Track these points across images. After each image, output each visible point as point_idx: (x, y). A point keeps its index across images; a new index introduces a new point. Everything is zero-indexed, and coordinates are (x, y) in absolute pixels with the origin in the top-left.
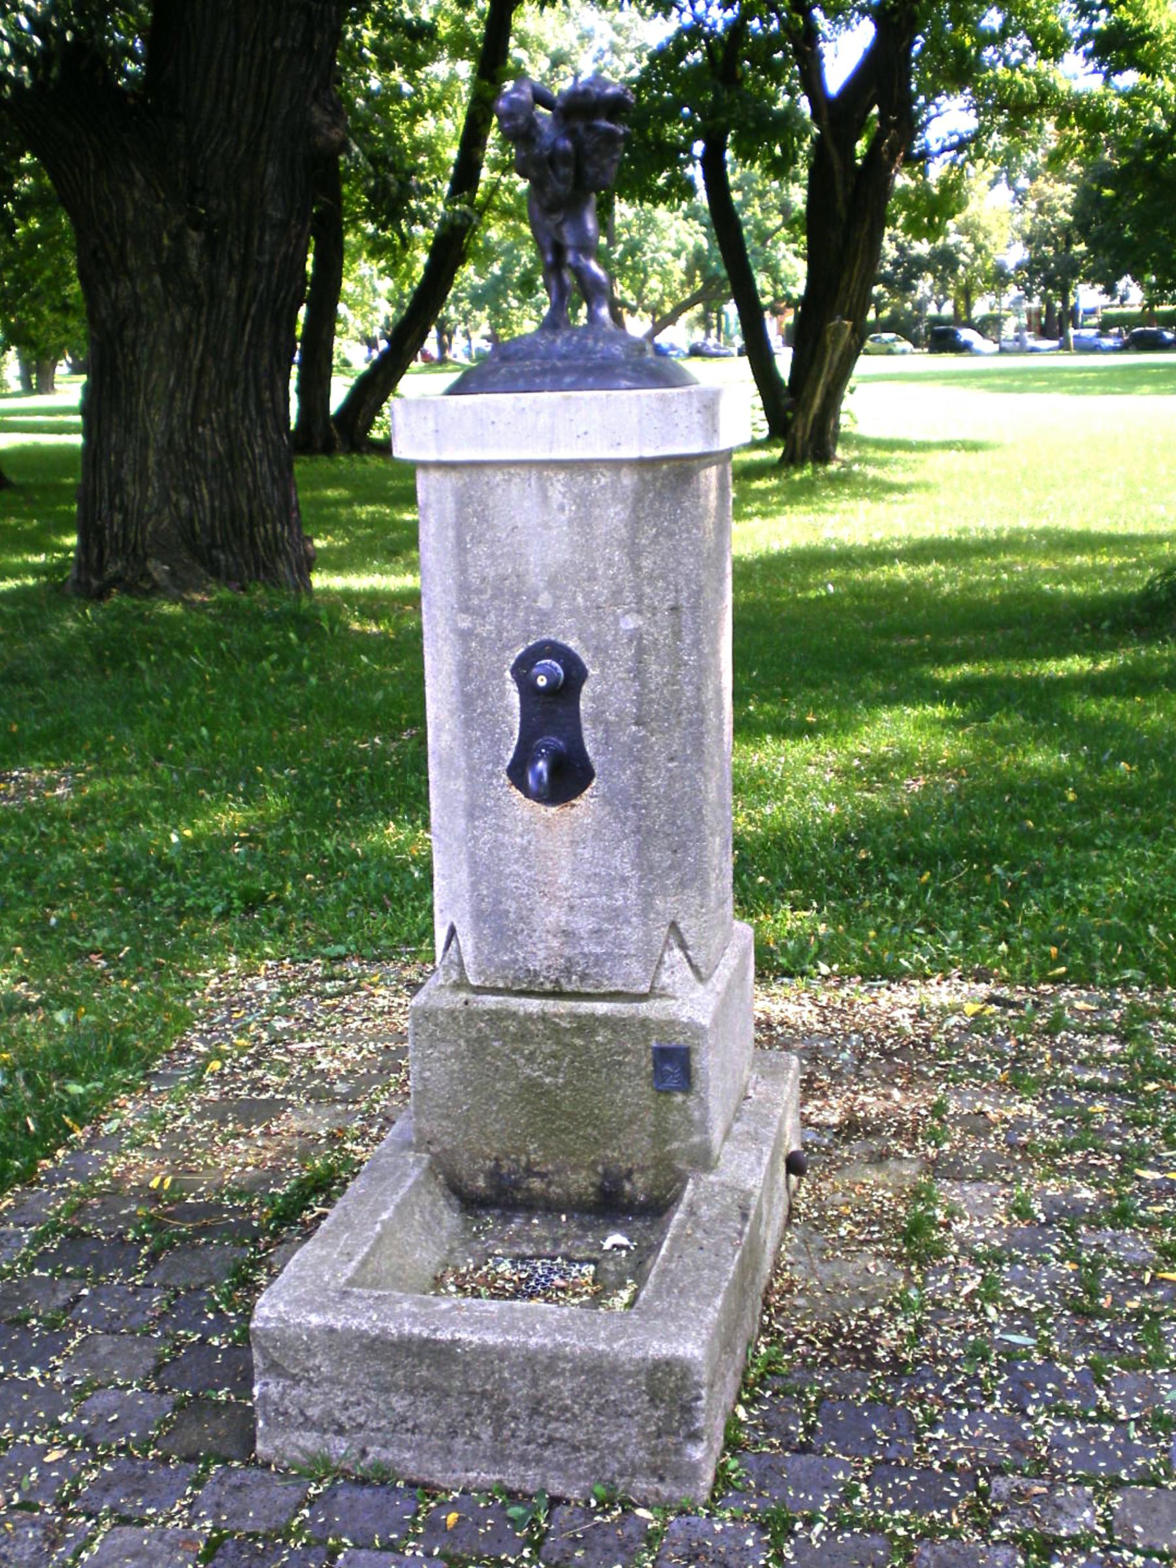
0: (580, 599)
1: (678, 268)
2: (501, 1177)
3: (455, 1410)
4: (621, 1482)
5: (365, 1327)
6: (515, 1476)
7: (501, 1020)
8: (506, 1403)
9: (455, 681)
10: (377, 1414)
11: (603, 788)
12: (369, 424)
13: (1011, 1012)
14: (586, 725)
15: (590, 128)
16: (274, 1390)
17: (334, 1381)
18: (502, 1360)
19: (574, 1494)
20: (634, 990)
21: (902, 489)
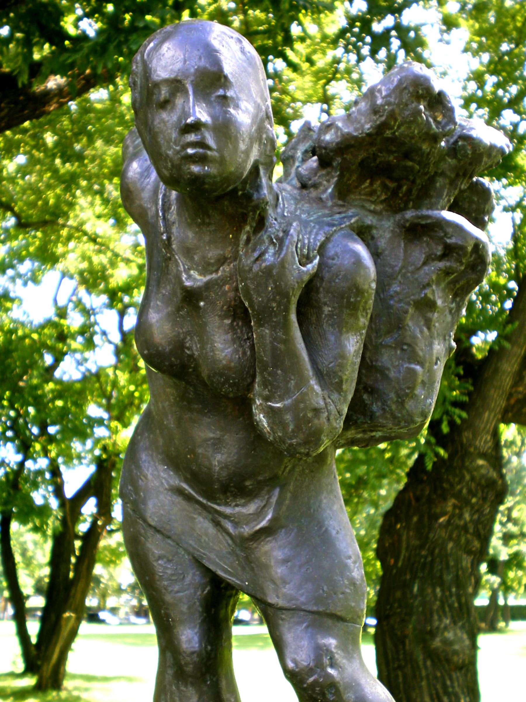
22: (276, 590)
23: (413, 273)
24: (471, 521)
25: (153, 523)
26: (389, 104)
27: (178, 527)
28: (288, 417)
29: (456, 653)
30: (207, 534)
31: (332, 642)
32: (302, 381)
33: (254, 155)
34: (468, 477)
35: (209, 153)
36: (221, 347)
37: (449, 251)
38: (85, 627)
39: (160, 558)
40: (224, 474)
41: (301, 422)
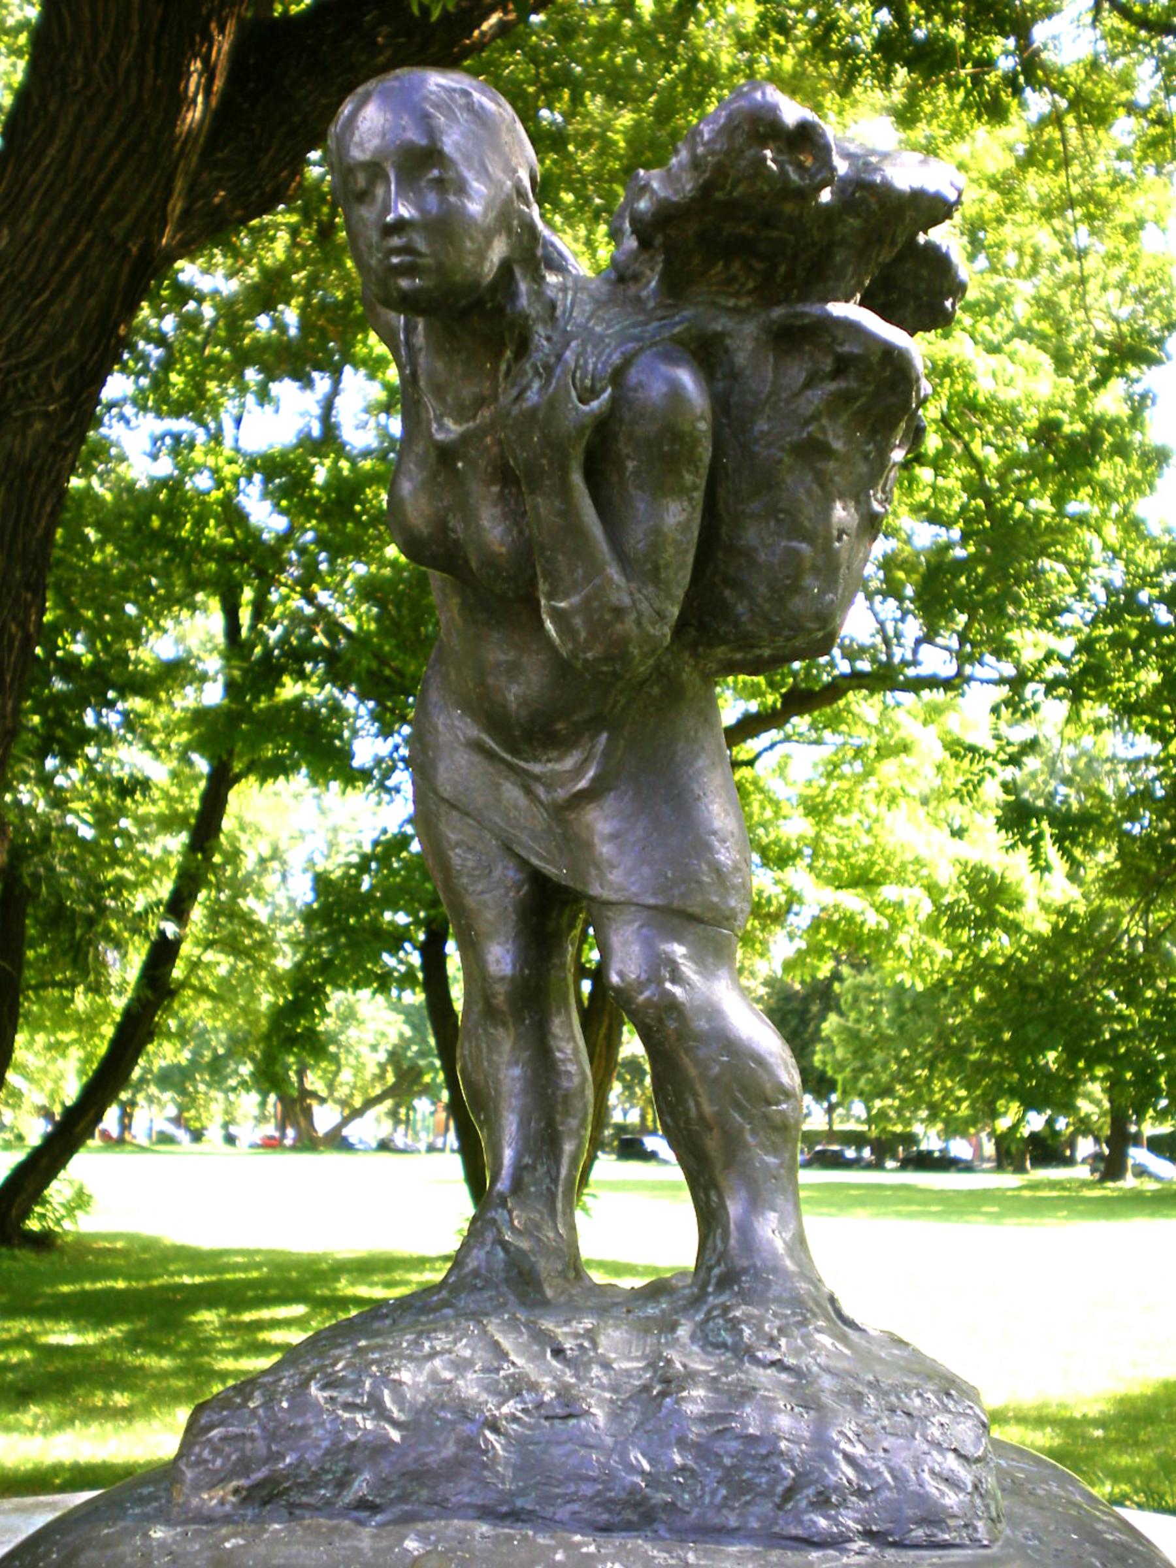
1: (372, 1061)
12: (26, 1213)
15: (793, 338)
22: (601, 878)
23: (788, 401)
25: (446, 795)
26: (713, 153)
27: (480, 800)
28: (578, 621)
30: (516, 807)
31: (679, 950)
32: (595, 569)
33: (499, 250)
35: (420, 261)
37: (843, 365)
38: (606, 1166)
39: (458, 844)
40: (524, 712)
41: (597, 628)
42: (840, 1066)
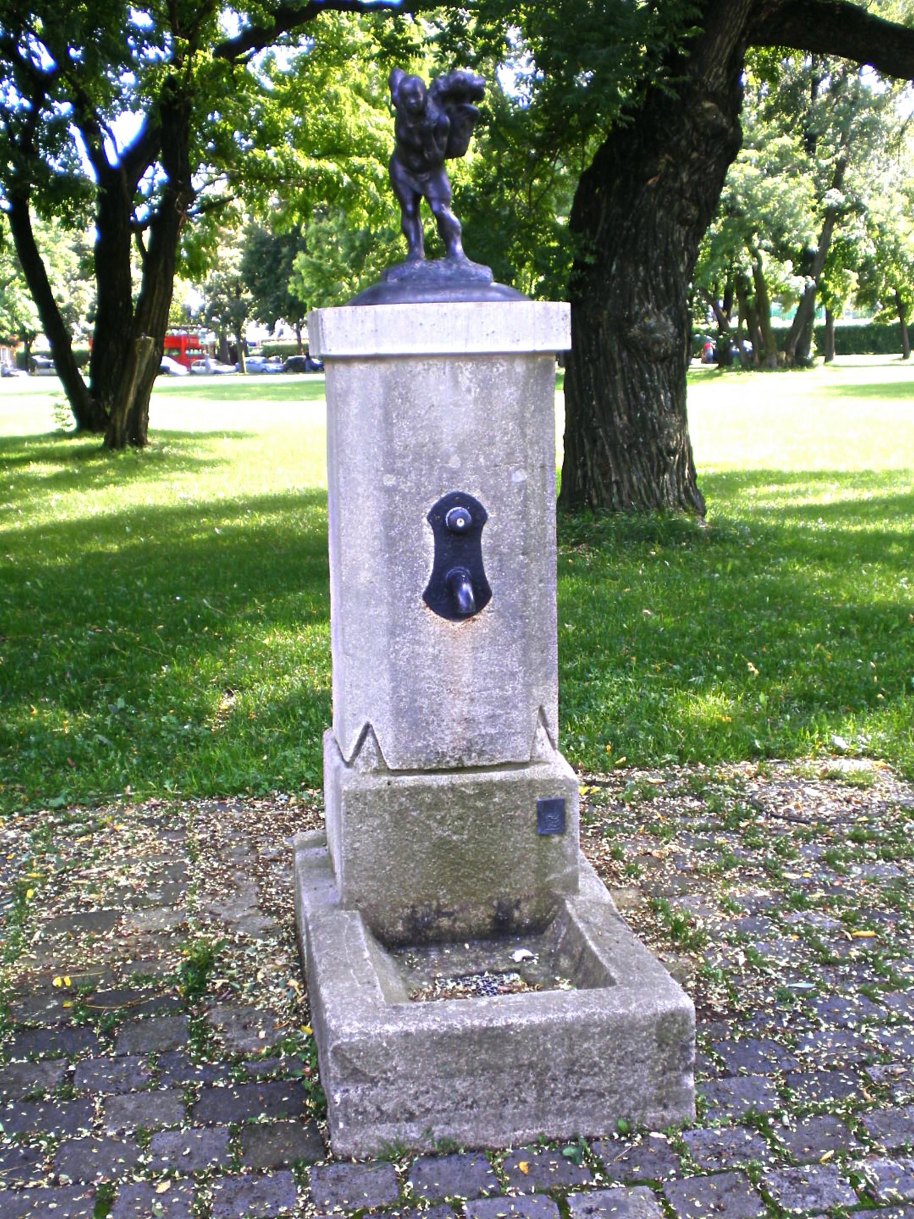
0: (482, 460)
2: (417, 920)
3: (507, 1082)
4: (636, 1116)
5: (434, 1027)
6: (557, 1126)
7: (419, 794)
8: (548, 1068)
9: (379, 528)
10: (443, 1097)
11: (498, 605)
13: (610, 790)
14: (485, 557)
16: (354, 1094)
17: (405, 1077)
18: (545, 1035)
19: (600, 1132)
20: (520, 760)
21: (212, 464)
24: (689, 181)
29: (658, 342)
34: (688, 126)
36: (418, 141)
42: (308, 293)
